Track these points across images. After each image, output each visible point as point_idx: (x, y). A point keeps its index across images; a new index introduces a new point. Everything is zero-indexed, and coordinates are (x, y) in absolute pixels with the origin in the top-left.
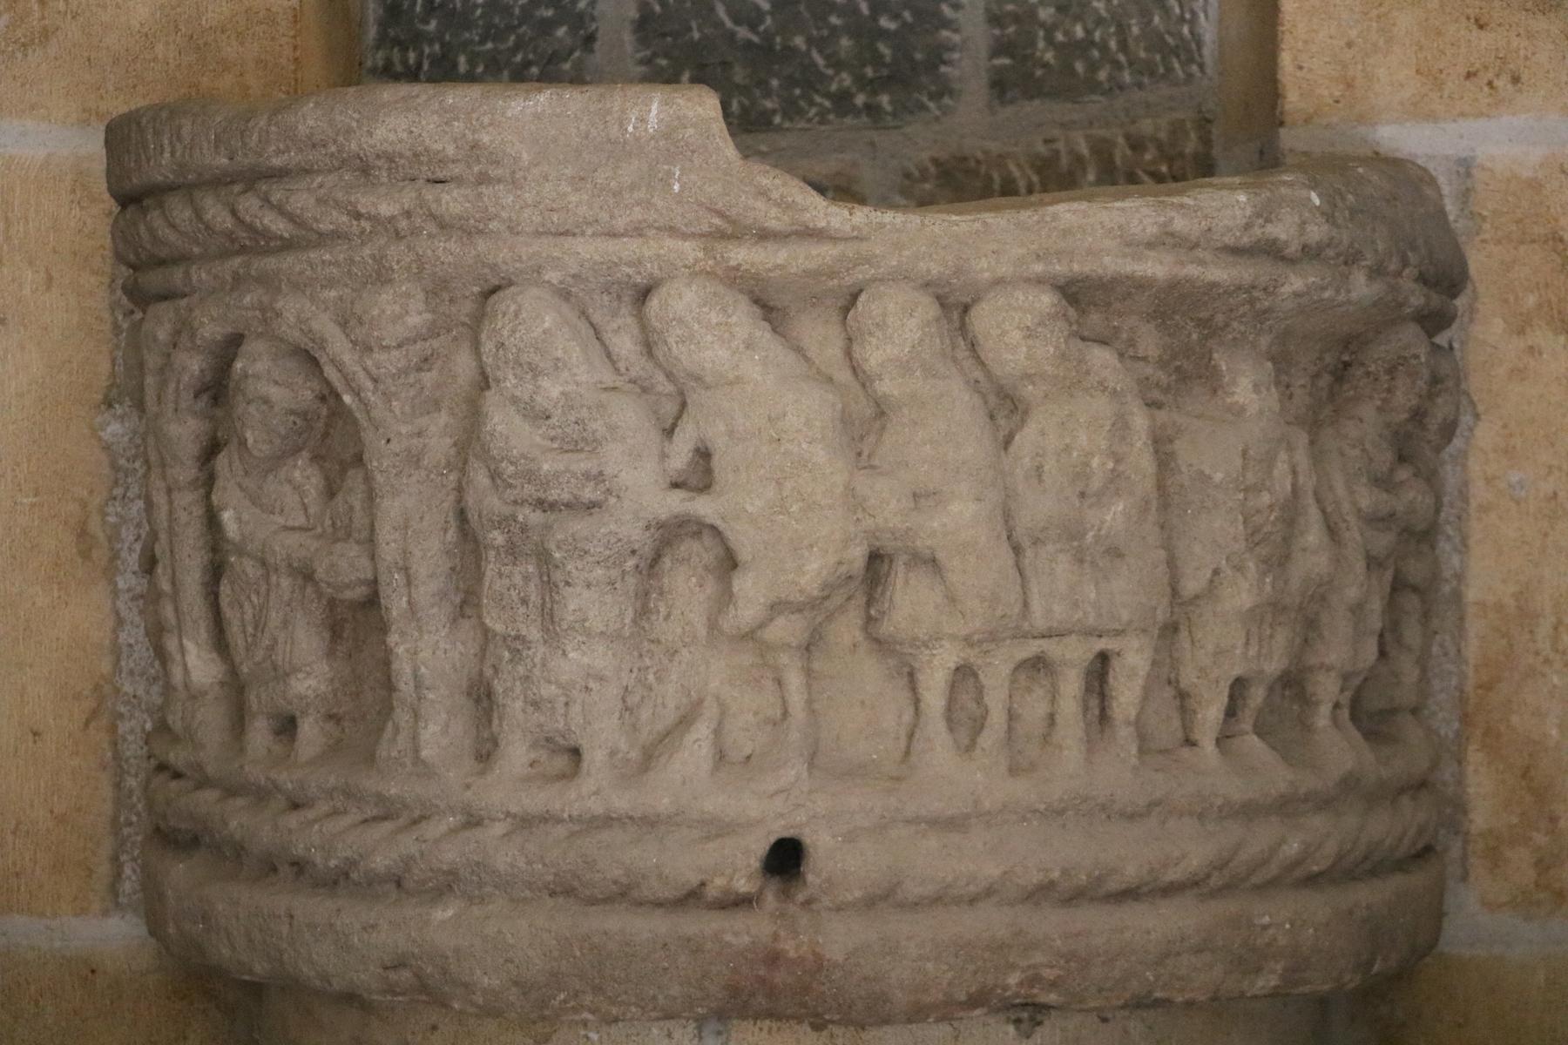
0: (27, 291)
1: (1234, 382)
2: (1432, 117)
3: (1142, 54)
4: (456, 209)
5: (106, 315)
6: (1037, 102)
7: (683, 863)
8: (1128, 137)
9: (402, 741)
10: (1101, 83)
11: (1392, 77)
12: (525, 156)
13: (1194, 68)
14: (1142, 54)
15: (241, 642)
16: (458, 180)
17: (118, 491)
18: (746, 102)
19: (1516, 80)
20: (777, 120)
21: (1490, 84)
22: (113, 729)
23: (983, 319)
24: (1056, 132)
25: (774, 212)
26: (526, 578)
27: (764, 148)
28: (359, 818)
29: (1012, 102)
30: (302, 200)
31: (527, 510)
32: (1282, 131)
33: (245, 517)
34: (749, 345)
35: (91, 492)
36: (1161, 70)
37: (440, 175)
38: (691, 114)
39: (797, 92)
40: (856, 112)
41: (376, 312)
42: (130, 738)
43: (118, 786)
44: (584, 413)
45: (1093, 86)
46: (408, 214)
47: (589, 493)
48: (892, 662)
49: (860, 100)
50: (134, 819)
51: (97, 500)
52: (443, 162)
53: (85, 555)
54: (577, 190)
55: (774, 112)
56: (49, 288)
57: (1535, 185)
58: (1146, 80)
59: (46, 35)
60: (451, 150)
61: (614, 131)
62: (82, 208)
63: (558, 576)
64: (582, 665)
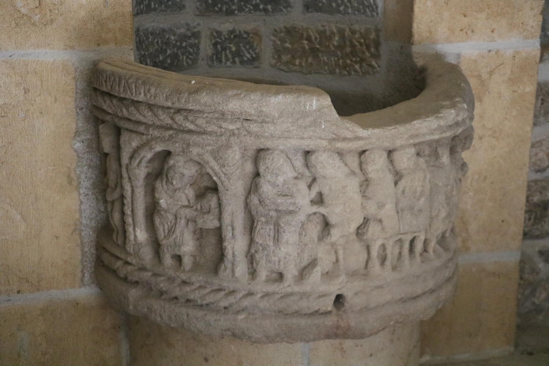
0: (49, 103)
1: (442, 156)
2: (451, 42)
3: (356, 5)
4: (255, 129)
5: (74, 110)
6: (319, 13)
7: (315, 305)
8: (350, 29)
9: (228, 271)
10: (341, 11)
11: (442, 31)
12: (276, 115)
13: (375, 13)
14: (356, 5)
15: (163, 235)
16: (256, 121)
17: (80, 164)
18: (227, 7)
19: (473, 31)
20: (236, 12)
21: (466, 33)
22: (80, 234)
23: (396, 156)
24: (325, 24)
25: (350, 133)
26: (270, 230)
27: (231, 20)
28: (211, 289)
29: (311, 12)
30: (201, 121)
31: (272, 212)
32: (413, 46)
33: (169, 202)
34: (339, 168)
35: (71, 164)
36: (362, 11)
37: (248, 118)
38: (325, 104)
39: (243, 3)
40: (260, 10)
41: (227, 156)
42: (86, 237)
43: (82, 251)
44: (290, 186)
45: (339, 12)
46: (238, 129)
47: (291, 208)
48: (362, 243)
49: (261, 7)
50: (88, 260)
51: (73, 167)
52: (250, 115)
53: (70, 183)
54: (293, 126)
55: (235, 10)
56: (56, 102)
57: (475, 61)
58: (356, 13)
59: (52, 21)
60: (253, 112)
61: (303, 108)
62: (65, 77)
63: (281, 230)
64: (287, 250)
